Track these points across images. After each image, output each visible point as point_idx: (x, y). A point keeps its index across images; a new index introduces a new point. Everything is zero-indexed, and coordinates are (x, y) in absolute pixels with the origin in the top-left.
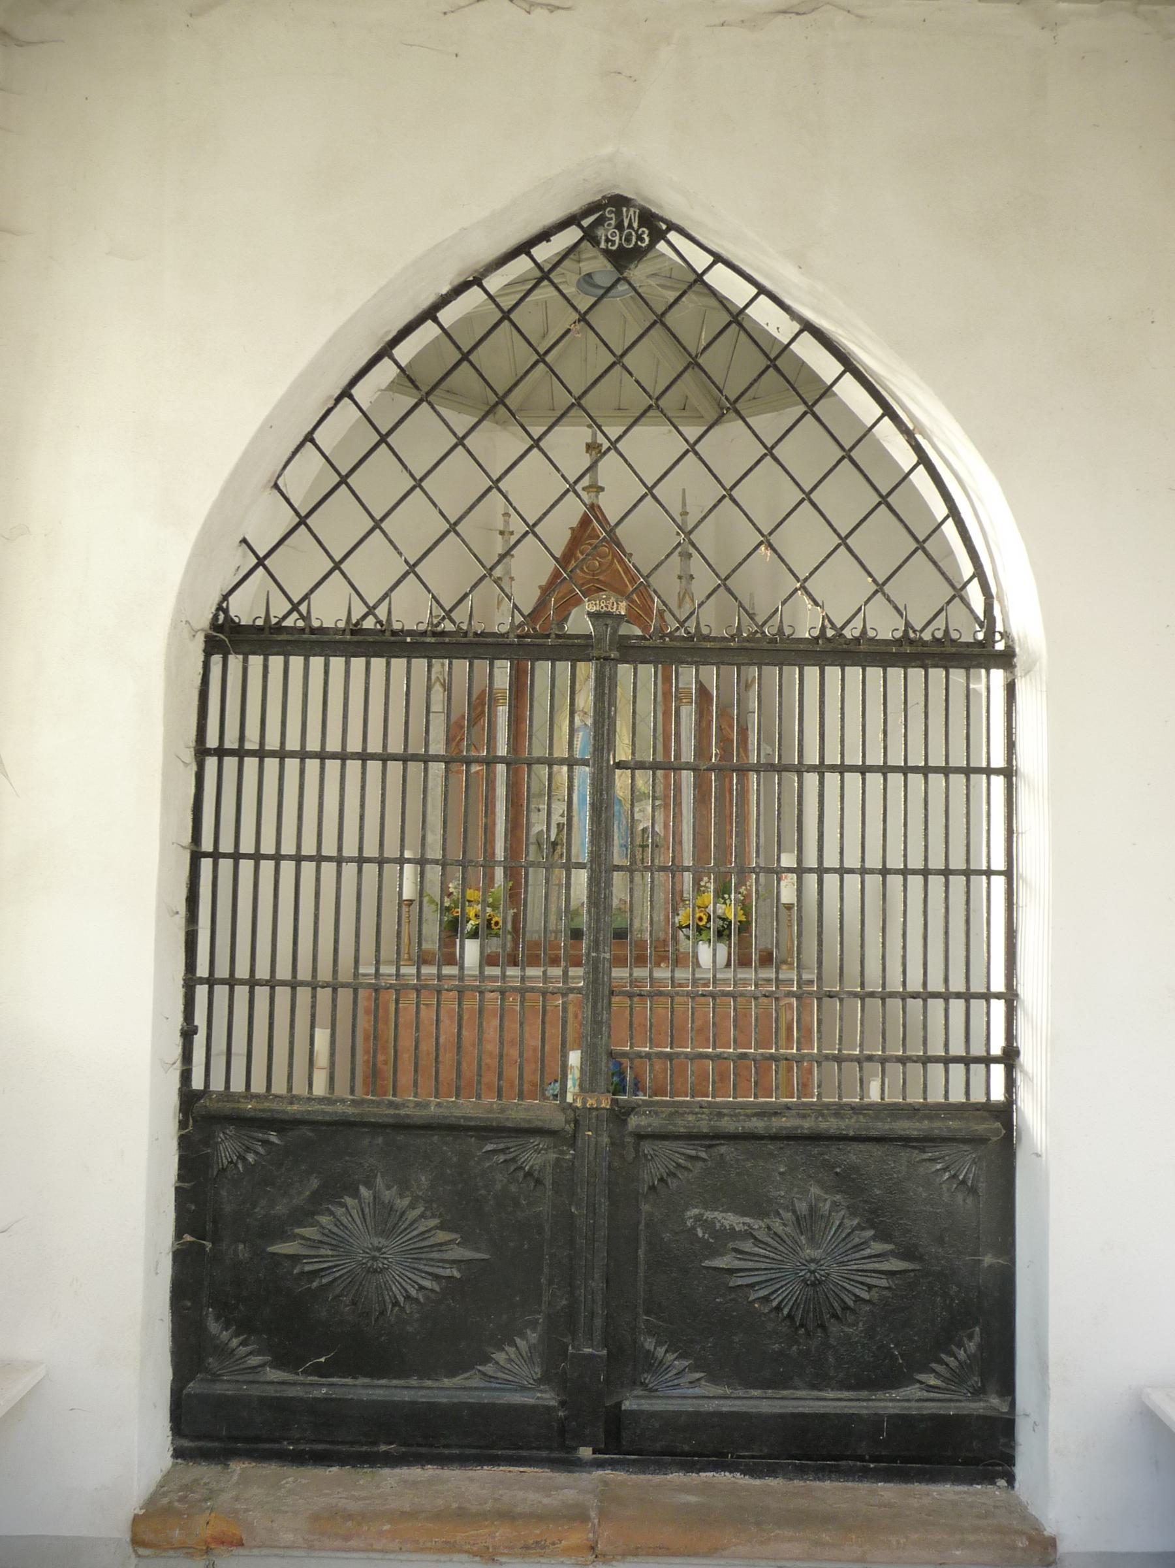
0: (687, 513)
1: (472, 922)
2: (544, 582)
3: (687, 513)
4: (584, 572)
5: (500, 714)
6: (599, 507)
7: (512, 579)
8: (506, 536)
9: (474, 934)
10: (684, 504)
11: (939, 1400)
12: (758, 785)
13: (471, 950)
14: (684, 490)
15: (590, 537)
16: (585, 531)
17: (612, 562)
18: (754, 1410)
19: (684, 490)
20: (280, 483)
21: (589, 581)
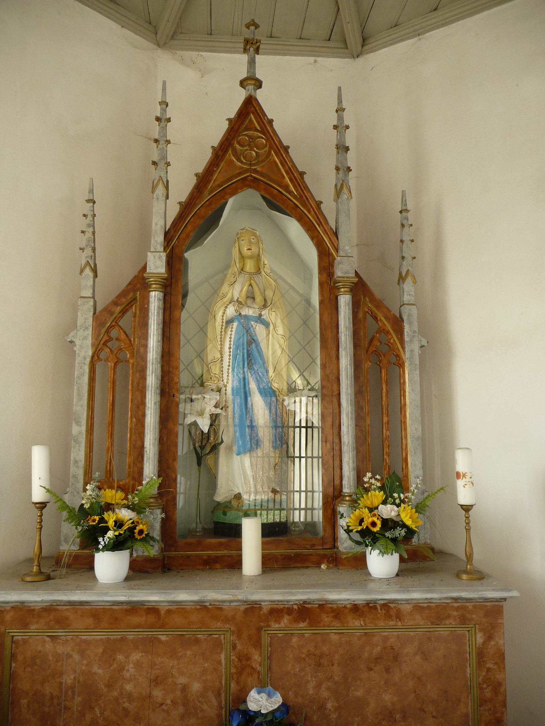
0: (344, 110)
1: (110, 534)
2: (200, 169)
3: (407, 211)
4: (241, 162)
5: (152, 300)
6: (256, 100)
7: (168, 164)
8: (163, 124)
9: (116, 545)
10: (340, 101)
11: (300, 46)
12: (300, 46)
13: (109, 566)
14: (340, 89)
15: (247, 129)
16: (242, 123)
17: (269, 153)
18: (351, 465)
19: (340, 89)
20: (327, 38)
21: (246, 171)
